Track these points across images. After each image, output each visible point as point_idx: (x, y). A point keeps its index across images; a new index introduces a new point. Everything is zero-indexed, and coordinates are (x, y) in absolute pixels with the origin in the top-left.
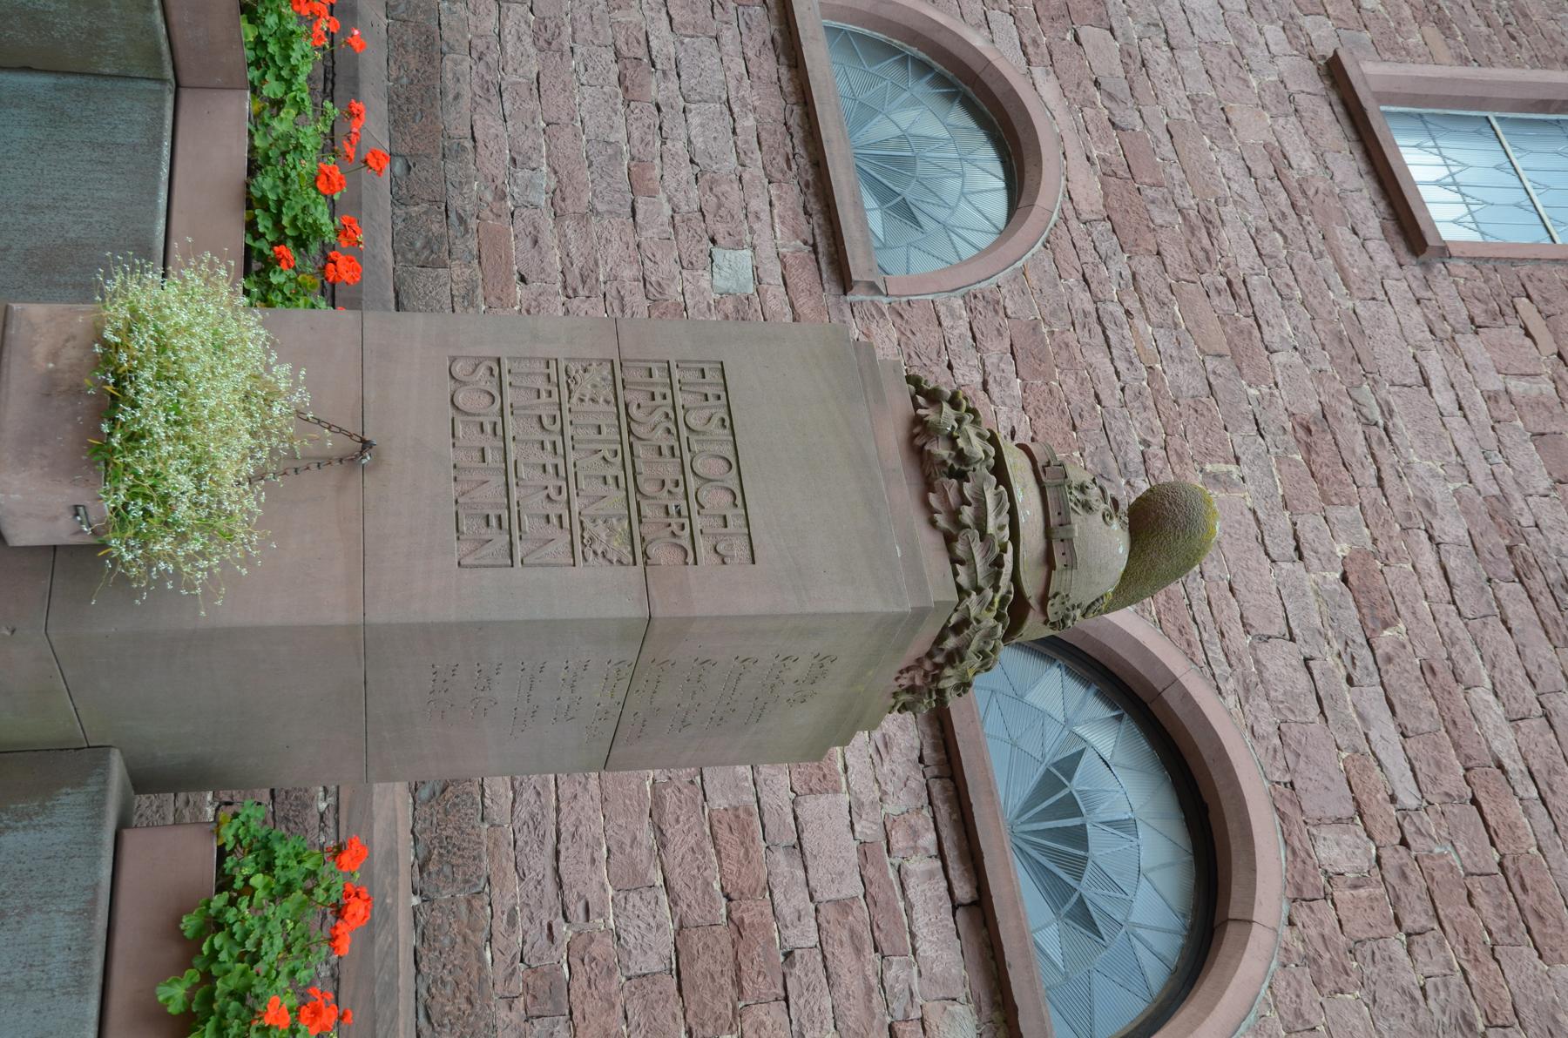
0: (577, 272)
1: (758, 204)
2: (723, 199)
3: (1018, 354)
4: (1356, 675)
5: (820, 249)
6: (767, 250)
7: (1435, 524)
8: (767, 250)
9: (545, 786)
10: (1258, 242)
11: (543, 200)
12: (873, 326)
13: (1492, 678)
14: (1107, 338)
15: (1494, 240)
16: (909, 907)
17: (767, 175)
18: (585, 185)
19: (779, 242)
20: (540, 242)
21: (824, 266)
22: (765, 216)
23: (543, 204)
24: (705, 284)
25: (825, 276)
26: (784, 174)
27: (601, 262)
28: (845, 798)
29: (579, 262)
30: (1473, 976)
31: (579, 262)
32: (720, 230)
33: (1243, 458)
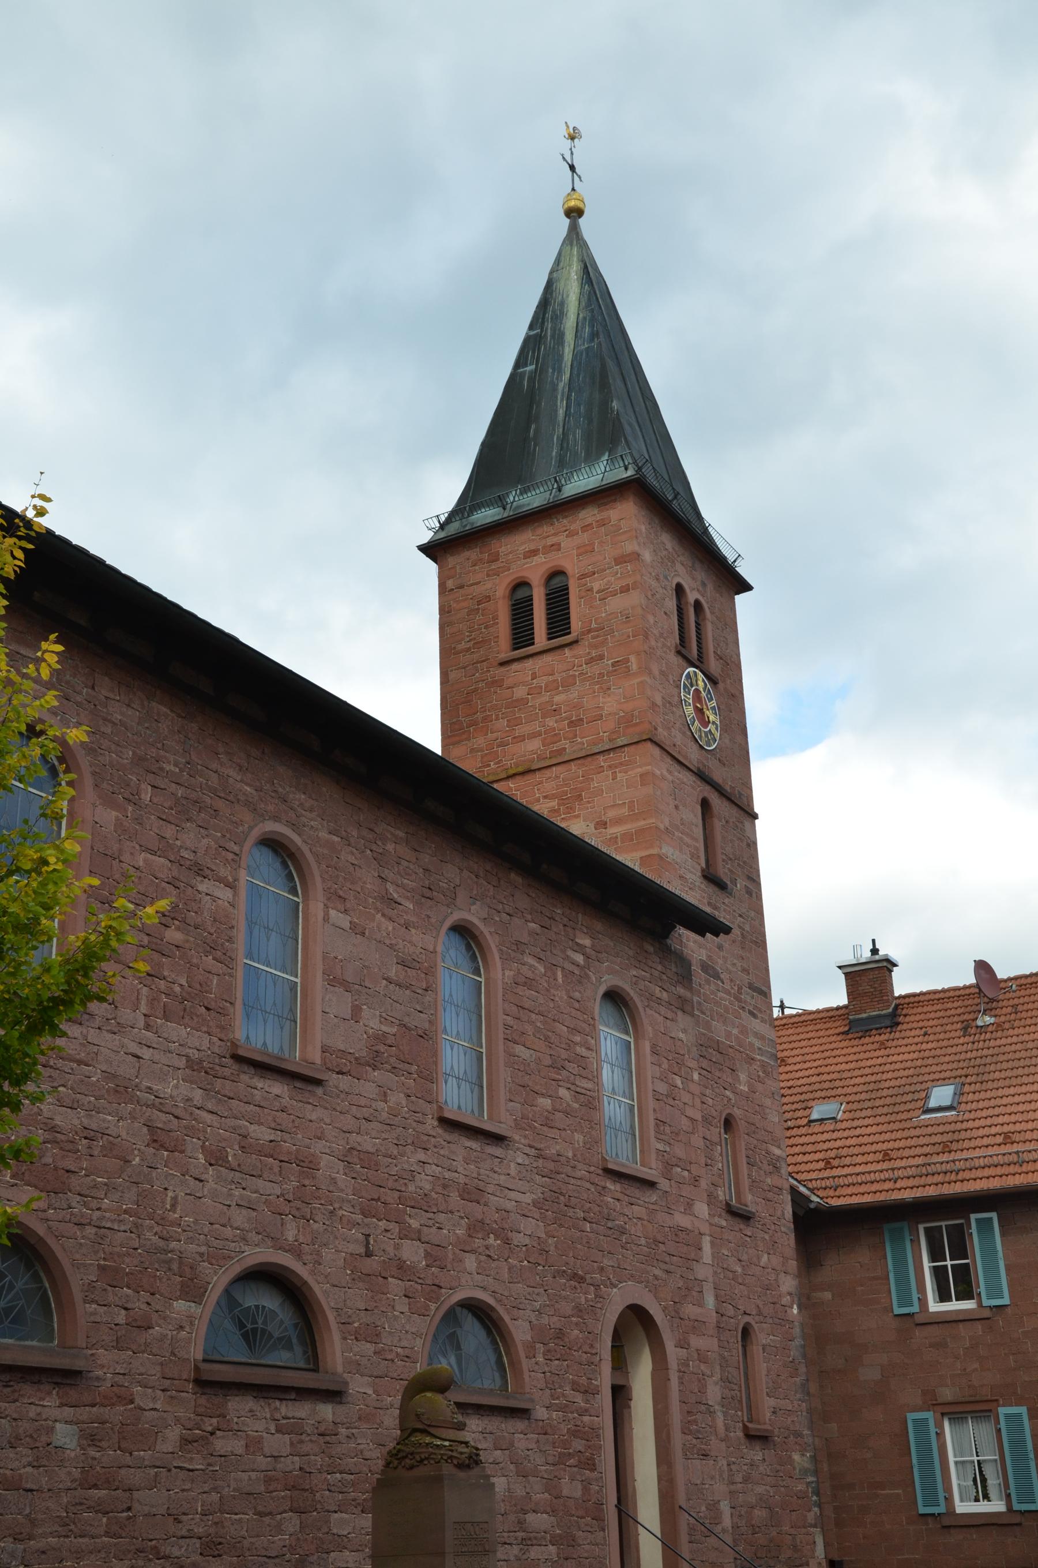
0: (60, 1529)
1: (32, 1412)
2: (27, 1433)
3: (115, 1284)
4: (244, 1185)
5: (59, 1381)
6: (56, 1413)
7: (195, 1103)
8: (56, 1413)
9: (252, 1560)
10: (65, 1104)
11: (20, 1547)
12: (99, 1362)
13: (247, 1121)
14: (109, 1228)
15: (794, 1012)
16: (293, 1418)
17: (14, 1402)
18: (13, 1518)
19: (54, 1404)
20: (44, 1549)
21: (68, 1382)
22: (39, 1409)
23: (22, 1547)
24: (73, 1454)
25: (73, 1382)
26: (14, 1391)
27: (58, 1514)
28: (264, 1434)
29: (56, 1528)
30: (323, 1202)
31: (56, 1528)
32: (44, 1439)
33: (166, 1186)
